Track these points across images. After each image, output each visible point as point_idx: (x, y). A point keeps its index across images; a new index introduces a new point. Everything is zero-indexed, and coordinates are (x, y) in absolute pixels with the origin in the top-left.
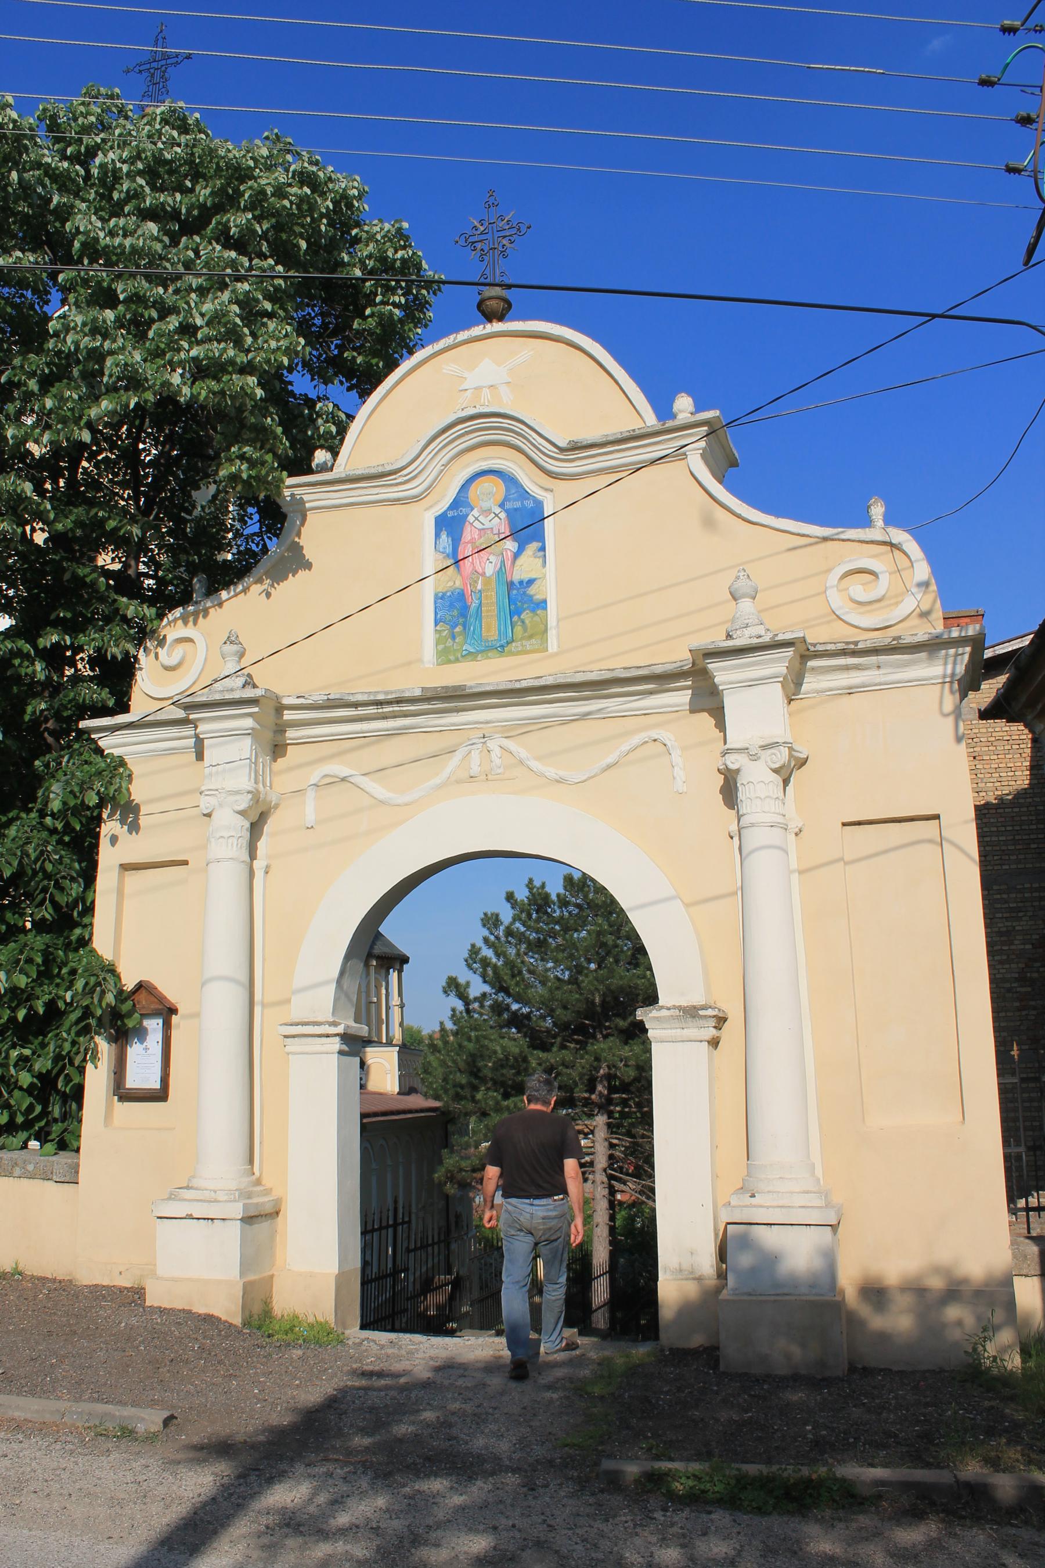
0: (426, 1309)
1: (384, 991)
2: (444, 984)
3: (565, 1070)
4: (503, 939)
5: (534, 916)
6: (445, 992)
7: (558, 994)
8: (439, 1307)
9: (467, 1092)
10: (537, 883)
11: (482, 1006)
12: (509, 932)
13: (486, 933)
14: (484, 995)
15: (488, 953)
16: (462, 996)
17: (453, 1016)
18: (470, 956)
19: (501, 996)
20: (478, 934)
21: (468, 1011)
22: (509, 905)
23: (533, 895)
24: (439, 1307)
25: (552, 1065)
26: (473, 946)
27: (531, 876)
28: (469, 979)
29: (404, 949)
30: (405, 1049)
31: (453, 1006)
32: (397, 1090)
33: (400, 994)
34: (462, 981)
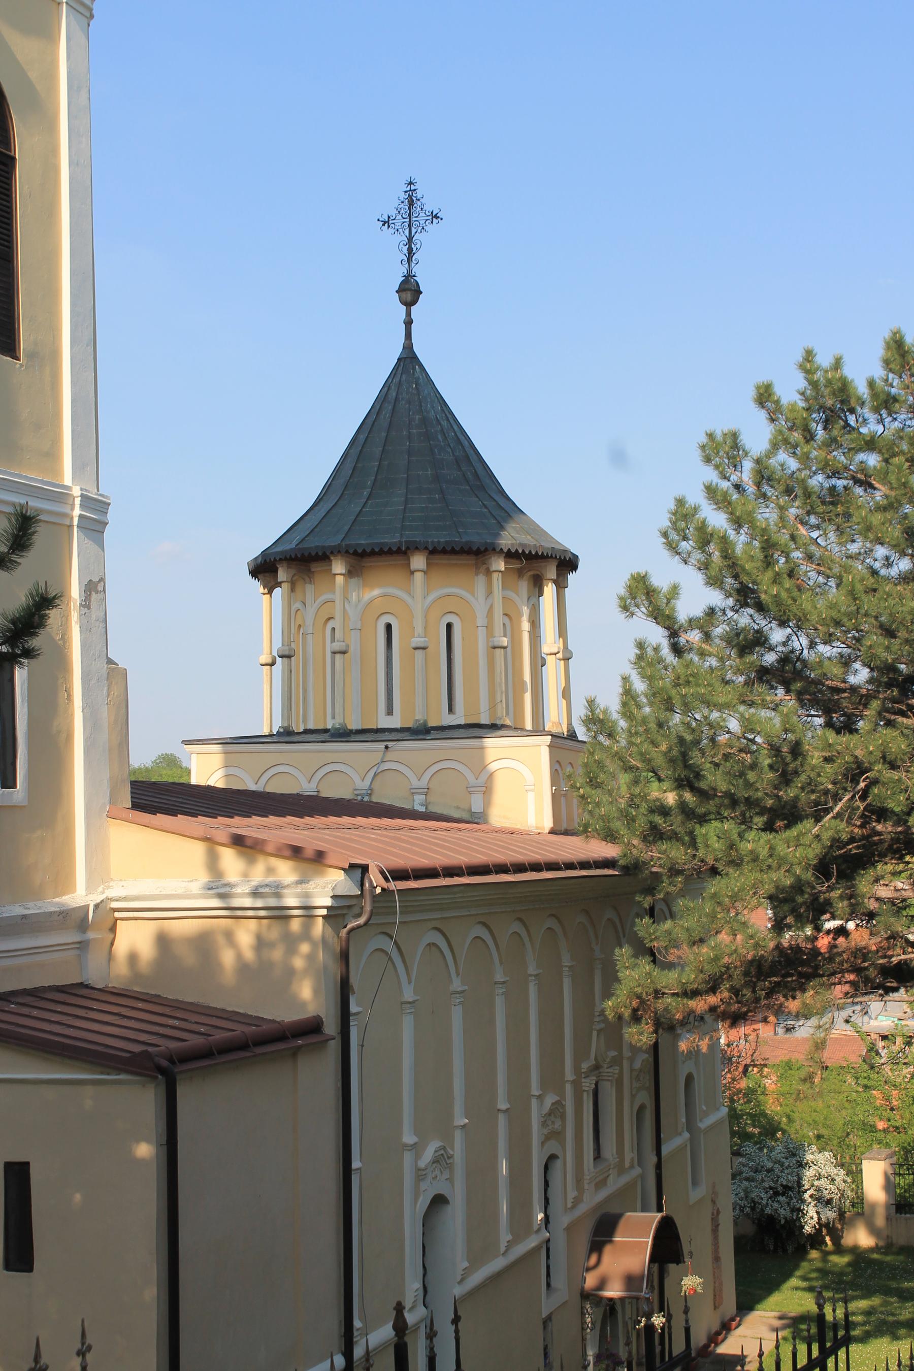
0: (602, 1284)
1: (526, 626)
2: (622, 591)
3: (890, 775)
4: (751, 489)
5: (820, 433)
6: (625, 608)
7: (869, 603)
8: (631, 1281)
9: (676, 823)
10: (824, 360)
11: (707, 637)
12: (763, 475)
13: (710, 475)
14: (711, 612)
15: (717, 520)
16: (662, 616)
17: (640, 658)
18: (674, 523)
19: (745, 619)
20: (694, 479)
21: (677, 650)
22: (763, 415)
23: (814, 384)
24: (631, 1281)
25: (858, 763)
26: (680, 502)
27: (810, 345)
28: (675, 579)
29: (567, 539)
30: (563, 742)
31: (640, 635)
32: (548, 824)
33: (562, 631)
34: (660, 581)
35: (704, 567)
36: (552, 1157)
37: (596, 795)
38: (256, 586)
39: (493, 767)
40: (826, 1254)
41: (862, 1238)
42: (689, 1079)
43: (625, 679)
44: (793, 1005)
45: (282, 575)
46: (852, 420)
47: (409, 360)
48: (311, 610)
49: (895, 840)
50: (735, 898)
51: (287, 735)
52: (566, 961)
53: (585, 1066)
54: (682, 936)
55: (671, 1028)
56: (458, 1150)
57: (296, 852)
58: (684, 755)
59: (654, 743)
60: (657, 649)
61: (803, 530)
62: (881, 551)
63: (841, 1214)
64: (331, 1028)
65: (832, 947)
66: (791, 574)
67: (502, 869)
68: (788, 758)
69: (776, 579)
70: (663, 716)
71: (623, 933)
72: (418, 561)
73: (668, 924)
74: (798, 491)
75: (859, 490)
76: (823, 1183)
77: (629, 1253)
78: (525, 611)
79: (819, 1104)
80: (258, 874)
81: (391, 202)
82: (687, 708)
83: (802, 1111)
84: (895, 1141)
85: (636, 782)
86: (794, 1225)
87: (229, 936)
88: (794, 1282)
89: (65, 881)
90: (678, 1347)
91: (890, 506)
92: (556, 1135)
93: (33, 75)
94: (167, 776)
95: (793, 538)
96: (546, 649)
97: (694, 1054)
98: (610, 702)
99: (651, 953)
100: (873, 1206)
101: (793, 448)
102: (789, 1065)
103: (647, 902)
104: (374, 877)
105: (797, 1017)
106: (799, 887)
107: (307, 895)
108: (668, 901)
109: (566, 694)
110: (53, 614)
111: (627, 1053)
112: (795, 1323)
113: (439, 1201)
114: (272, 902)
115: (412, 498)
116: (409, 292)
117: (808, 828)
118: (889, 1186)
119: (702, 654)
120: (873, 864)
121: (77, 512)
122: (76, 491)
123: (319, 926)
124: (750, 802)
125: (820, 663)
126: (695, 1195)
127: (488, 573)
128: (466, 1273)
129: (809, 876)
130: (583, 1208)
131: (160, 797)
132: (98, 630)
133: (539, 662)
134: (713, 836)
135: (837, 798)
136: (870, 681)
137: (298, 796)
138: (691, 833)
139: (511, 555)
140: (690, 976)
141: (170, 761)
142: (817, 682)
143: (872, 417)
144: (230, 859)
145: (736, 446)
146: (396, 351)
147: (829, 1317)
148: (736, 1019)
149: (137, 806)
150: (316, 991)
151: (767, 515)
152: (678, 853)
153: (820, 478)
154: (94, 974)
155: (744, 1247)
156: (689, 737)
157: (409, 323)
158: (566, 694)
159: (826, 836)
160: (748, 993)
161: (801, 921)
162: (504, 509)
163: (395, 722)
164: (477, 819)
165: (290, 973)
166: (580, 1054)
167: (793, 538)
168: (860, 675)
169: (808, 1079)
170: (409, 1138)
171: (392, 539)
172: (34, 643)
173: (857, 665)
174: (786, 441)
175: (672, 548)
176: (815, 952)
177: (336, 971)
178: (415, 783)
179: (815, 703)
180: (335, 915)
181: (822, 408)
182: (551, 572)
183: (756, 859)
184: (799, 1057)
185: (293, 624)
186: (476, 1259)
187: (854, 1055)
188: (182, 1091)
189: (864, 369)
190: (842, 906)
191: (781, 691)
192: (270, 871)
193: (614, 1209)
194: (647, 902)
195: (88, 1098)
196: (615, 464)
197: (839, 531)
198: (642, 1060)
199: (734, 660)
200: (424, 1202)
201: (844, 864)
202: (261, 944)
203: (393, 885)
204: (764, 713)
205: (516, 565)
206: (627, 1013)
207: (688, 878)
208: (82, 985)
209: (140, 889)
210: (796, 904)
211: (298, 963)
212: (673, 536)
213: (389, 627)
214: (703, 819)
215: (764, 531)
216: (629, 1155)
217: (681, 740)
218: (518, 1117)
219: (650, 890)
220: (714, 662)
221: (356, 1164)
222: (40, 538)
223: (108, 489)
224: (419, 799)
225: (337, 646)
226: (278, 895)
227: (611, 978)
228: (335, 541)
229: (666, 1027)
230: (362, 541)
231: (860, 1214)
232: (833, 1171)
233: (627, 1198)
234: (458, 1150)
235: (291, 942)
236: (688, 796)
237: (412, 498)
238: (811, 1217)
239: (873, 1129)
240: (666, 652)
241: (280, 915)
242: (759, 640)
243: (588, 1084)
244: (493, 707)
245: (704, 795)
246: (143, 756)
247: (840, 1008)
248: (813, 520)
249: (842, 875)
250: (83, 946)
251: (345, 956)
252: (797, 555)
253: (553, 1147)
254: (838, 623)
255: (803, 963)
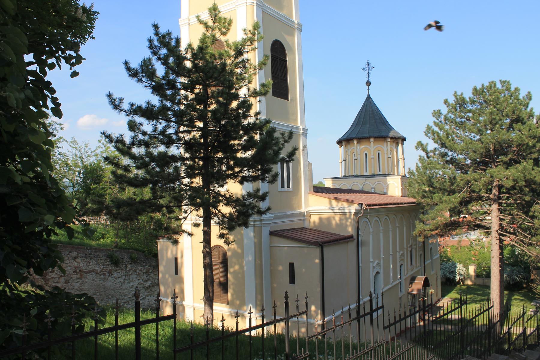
0: (412, 291)
1: (395, 153)
2: (416, 145)
4: (443, 122)
5: (458, 109)
6: (417, 148)
7: (470, 146)
8: (419, 290)
9: (428, 194)
10: (459, 93)
11: (435, 154)
12: (446, 119)
13: (434, 119)
14: (435, 149)
15: (436, 129)
16: (425, 150)
17: (420, 159)
19: (443, 150)
20: (431, 120)
21: (428, 157)
22: (446, 106)
23: (457, 99)
26: (428, 125)
27: (456, 90)
29: (403, 134)
30: (404, 177)
31: (420, 154)
32: (400, 195)
33: (403, 154)
34: (424, 142)
35: (434, 139)
36: (402, 264)
37: (411, 188)
38: (338, 146)
39: (388, 183)
40: (461, 286)
41: (469, 282)
42: (431, 248)
43: (417, 164)
44: (454, 233)
45: (343, 143)
46: (465, 106)
47: (369, 98)
48: (349, 151)
49: (477, 197)
50: (441, 210)
51: (345, 177)
52: (405, 224)
53: (409, 246)
54: (430, 218)
55: (427, 238)
56: (382, 262)
57: (347, 201)
58: (430, 180)
59: (423, 177)
60: (424, 157)
61: (455, 130)
62: (473, 135)
63: (464, 278)
64: (355, 237)
65: (463, 220)
66: (453, 140)
67: (391, 204)
68: (453, 180)
69: (450, 141)
70: (425, 171)
71: (417, 217)
72: (372, 140)
73: (427, 216)
74: (454, 122)
75: (467, 121)
76: (460, 271)
77: (418, 284)
78: (395, 150)
79: (460, 254)
80: (340, 205)
81: (364, 65)
82: (430, 169)
83: (456, 255)
84: (476, 262)
85: (419, 186)
86: (454, 279)
87: (334, 218)
88: (454, 291)
89: (300, 206)
90: (430, 303)
91: (475, 125)
92: (403, 260)
93: (290, 44)
94: (320, 186)
95: (453, 132)
96: (399, 158)
97: (432, 243)
98: (414, 169)
99: (423, 222)
100: (472, 276)
101: (452, 113)
102: (453, 246)
103: (422, 211)
104: (364, 206)
105: (455, 235)
106: (455, 207)
107: (350, 210)
108: (426, 211)
109: (404, 167)
110: (297, 152)
111: (418, 243)
112: (454, 300)
113: (378, 273)
114: (343, 211)
115: (370, 127)
116: (369, 83)
117: (457, 195)
118: (475, 272)
119: (434, 158)
120: (472, 203)
121: (301, 131)
122: (301, 127)
123: (352, 216)
124: (444, 190)
125: (460, 159)
126: (432, 273)
127: (387, 142)
128: (383, 288)
129: (458, 205)
130: (408, 275)
131: (319, 190)
132: (306, 155)
133: (398, 161)
134: (437, 197)
135: (464, 188)
136: (471, 163)
137: (348, 189)
138: (432, 196)
139: (392, 138)
140: (431, 227)
141: (321, 183)
142: (458, 163)
143: (470, 105)
144: (334, 202)
145: (440, 113)
146: (366, 96)
147: (462, 299)
148: (441, 236)
149: (314, 191)
150: (352, 230)
151: (447, 127)
152: (429, 201)
153: (459, 119)
154: (306, 226)
155: (442, 284)
156: (431, 176)
157: (369, 90)
158: (404, 167)
159: (461, 196)
160: (444, 231)
161: (456, 215)
162: (390, 128)
163: (367, 174)
164: (385, 194)
165: (347, 226)
166: (407, 244)
167: (453, 132)
168: (468, 162)
169: (457, 248)
170: (371, 260)
171: (366, 135)
172: (293, 158)
173: (468, 159)
174: (451, 111)
175: (427, 135)
176: (459, 222)
177: (356, 225)
178: (372, 186)
179: (458, 168)
180: (356, 214)
181: (459, 104)
182: (400, 141)
183: (446, 201)
184: (455, 244)
185: (345, 152)
186: (385, 285)
187: (467, 244)
188: (325, 249)
189: (468, 95)
190: (465, 212)
191: (451, 165)
192: (342, 204)
193: (415, 276)
194: (422, 211)
195: (306, 250)
196: (413, 118)
197: (463, 130)
198: (421, 244)
199: (440, 159)
200: (375, 273)
201: (465, 203)
202: (340, 219)
203: (368, 207)
204: (447, 170)
205: (393, 140)
206: (418, 235)
207: (431, 206)
208: (304, 228)
209: (316, 209)
210: (455, 211)
211: (348, 223)
212: (427, 133)
213: (366, 154)
214: (434, 193)
215: (447, 131)
216: (418, 264)
217: (429, 176)
218: (394, 256)
219: (423, 209)
220: (436, 159)
221: (360, 265)
222: (294, 137)
223: (307, 127)
224: (373, 190)
225: (355, 158)
226: (344, 210)
227: (414, 227)
228: (354, 136)
229: (426, 237)
230: (360, 136)
231: (469, 278)
232: (463, 268)
233: (418, 273)
234: (382, 262)
235: (347, 219)
236: (431, 189)
237: (370, 127)
238: (458, 278)
239: (471, 259)
240: (425, 157)
241: (344, 214)
242: (446, 155)
243: (409, 249)
244: (388, 170)
245: (434, 188)
246: (315, 182)
247: (465, 234)
248: (457, 128)
249: (465, 205)
250: (304, 220)
251: (358, 222)
252: (454, 136)
253: (402, 262)
254: (463, 150)
255: (456, 224)
